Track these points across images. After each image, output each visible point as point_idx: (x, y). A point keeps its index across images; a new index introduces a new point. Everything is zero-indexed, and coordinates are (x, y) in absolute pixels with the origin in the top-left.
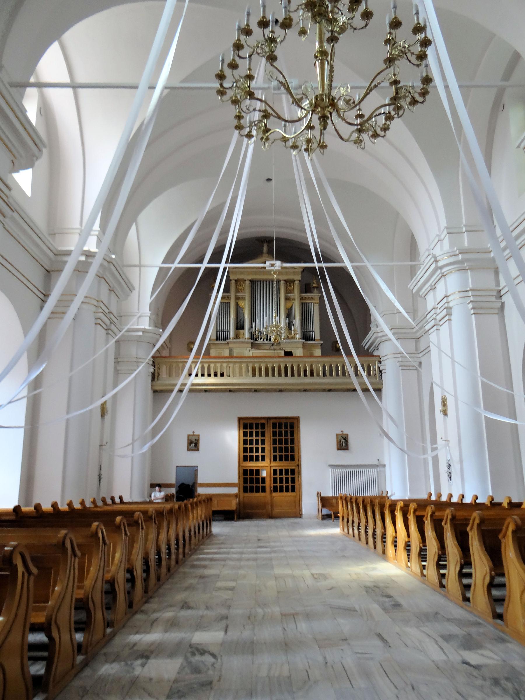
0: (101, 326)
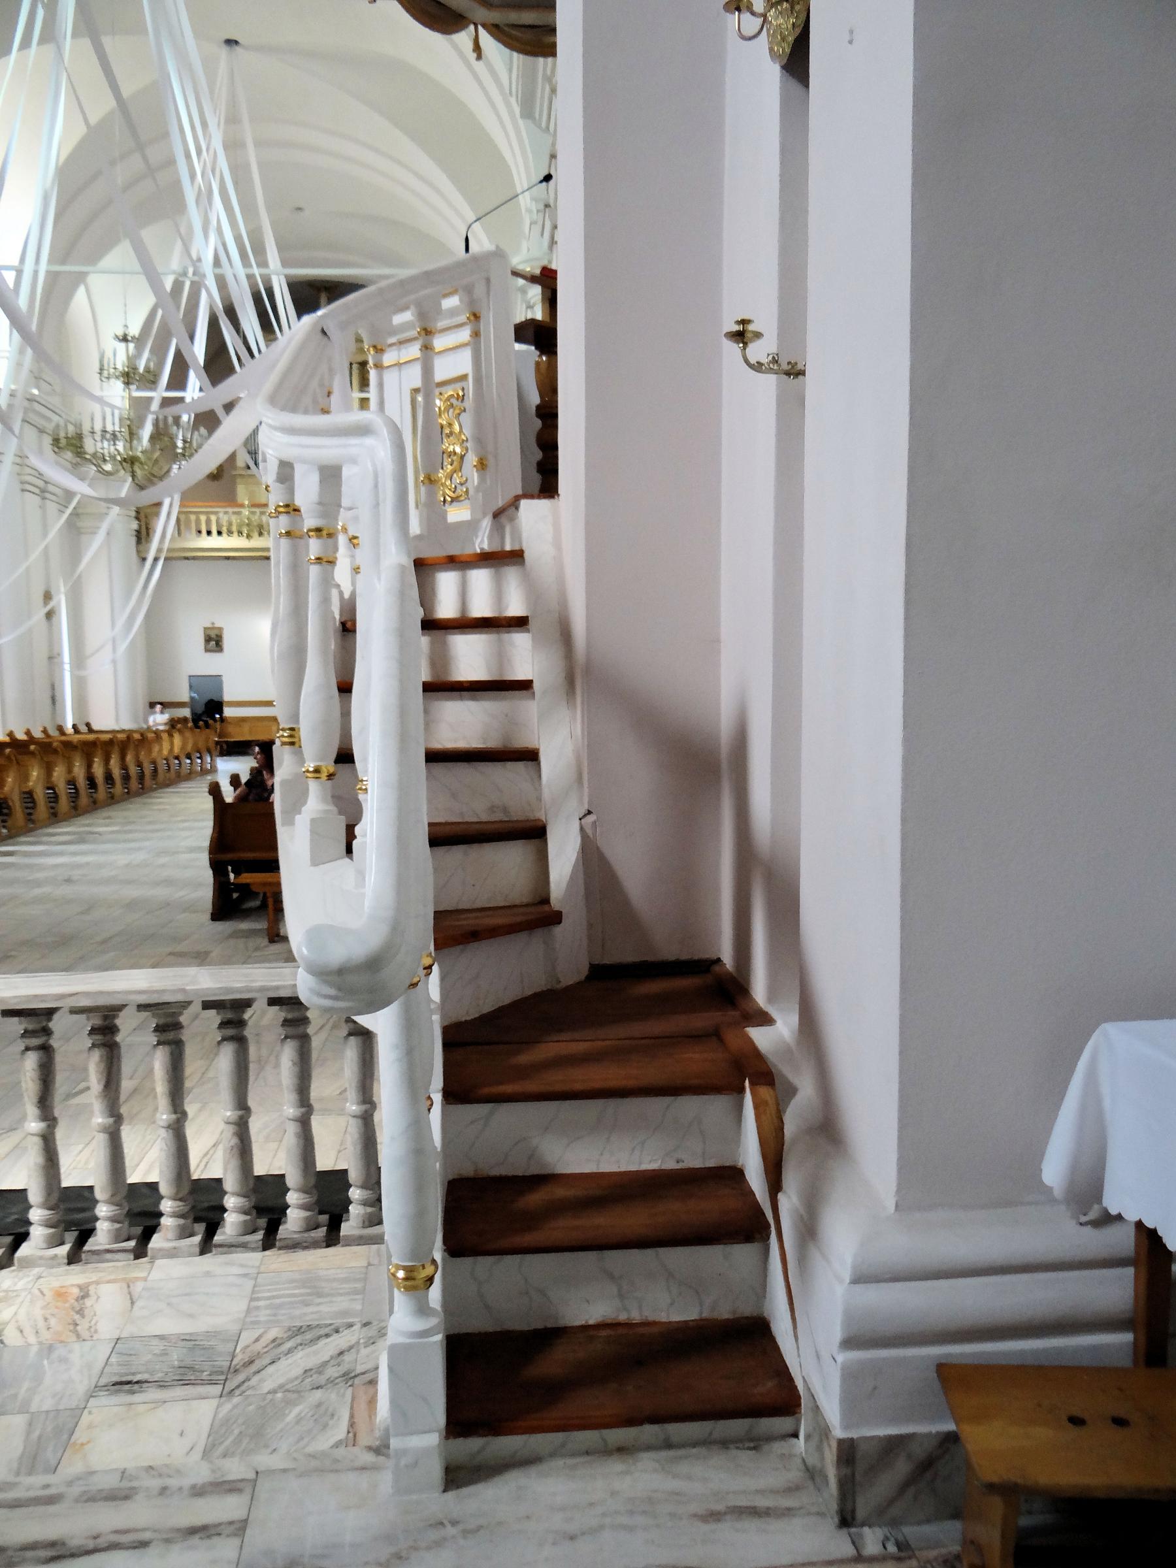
0: (30, 492)
